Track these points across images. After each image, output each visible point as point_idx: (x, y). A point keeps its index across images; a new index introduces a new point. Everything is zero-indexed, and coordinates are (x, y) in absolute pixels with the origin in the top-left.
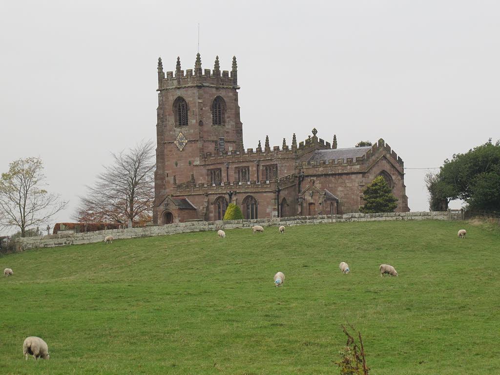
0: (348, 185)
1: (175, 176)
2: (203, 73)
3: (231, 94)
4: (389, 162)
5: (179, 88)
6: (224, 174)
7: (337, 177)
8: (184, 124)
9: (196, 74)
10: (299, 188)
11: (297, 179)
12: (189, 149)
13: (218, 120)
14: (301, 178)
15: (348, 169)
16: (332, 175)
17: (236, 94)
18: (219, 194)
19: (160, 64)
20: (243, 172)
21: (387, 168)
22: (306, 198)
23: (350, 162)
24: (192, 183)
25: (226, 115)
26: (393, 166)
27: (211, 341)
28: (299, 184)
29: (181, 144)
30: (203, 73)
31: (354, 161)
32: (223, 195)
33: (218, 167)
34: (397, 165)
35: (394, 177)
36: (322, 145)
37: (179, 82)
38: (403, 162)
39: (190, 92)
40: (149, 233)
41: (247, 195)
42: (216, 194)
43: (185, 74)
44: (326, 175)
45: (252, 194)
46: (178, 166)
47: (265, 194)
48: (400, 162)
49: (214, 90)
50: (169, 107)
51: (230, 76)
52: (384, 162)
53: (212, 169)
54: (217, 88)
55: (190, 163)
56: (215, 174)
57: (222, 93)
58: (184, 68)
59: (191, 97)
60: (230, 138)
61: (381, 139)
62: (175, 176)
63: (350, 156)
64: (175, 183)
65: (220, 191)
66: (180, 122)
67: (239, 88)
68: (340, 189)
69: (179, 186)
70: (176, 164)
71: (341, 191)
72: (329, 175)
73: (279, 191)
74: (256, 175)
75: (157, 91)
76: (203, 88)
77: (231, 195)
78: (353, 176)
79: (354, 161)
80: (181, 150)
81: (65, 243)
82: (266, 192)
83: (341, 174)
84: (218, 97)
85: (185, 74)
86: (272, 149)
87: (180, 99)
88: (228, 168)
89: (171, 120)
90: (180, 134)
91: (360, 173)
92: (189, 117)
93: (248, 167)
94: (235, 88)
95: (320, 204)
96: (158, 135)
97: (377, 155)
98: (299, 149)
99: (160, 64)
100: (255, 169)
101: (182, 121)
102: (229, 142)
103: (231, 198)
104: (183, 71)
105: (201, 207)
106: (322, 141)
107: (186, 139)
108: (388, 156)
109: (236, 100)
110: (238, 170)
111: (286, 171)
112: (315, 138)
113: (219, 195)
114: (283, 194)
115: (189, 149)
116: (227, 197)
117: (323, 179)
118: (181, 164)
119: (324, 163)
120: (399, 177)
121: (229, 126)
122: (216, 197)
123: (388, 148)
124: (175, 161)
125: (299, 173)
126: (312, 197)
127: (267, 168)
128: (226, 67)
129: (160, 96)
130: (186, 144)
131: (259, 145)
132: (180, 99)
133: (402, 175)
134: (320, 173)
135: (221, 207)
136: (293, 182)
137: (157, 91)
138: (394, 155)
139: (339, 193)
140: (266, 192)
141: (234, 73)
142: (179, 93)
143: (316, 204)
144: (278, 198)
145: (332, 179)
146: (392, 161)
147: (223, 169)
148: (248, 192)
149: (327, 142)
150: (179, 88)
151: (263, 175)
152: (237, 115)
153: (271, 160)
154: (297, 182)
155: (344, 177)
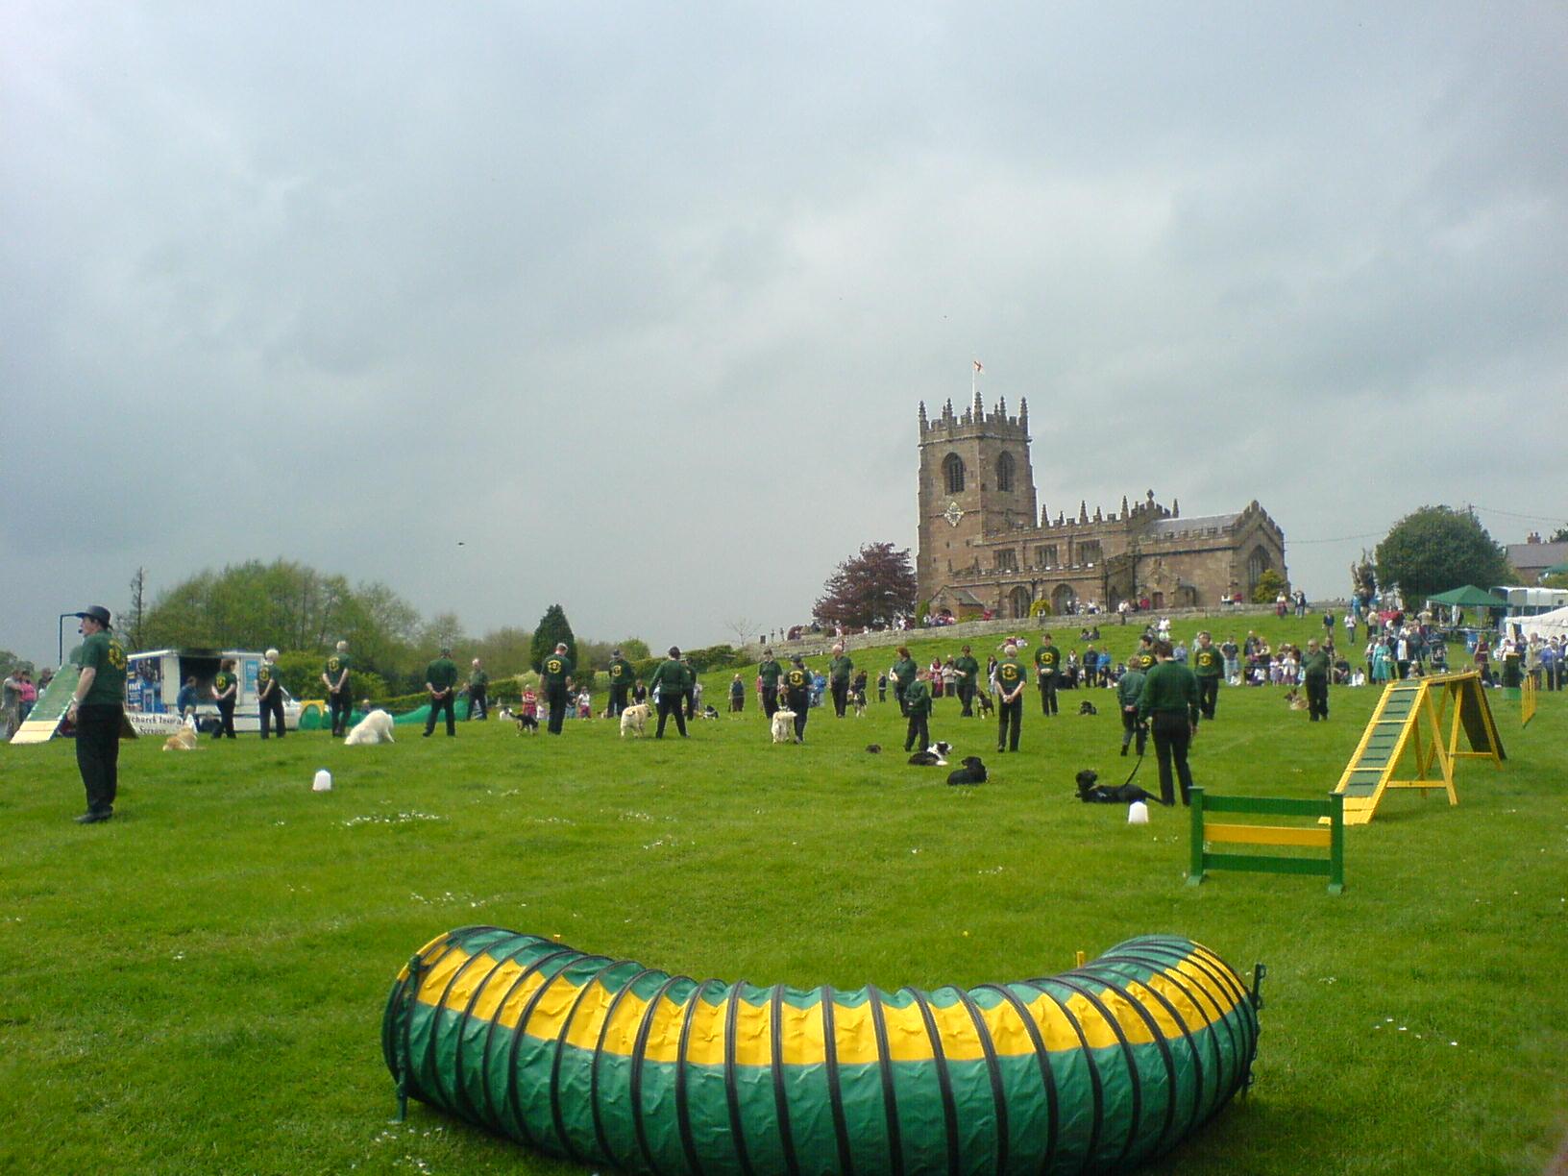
0: (1210, 566)
1: (949, 561)
2: (985, 420)
3: (1020, 449)
4: (1265, 533)
5: (950, 441)
6: (1019, 557)
7: (1193, 555)
8: (957, 491)
9: (1020, 423)
10: (1134, 572)
11: (1131, 559)
12: (966, 523)
13: (1004, 486)
14: (1139, 558)
15: (1212, 543)
16: (1187, 553)
17: (1027, 449)
18: (1018, 583)
19: (922, 409)
20: (1048, 553)
21: (1264, 542)
22: (1148, 585)
23: (1213, 532)
24: (973, 570)
25: (1015, 477)
26: (1271, 539)
27: (699, 880)
28: (1134, 567)
29: (954, 517)
30: (985, 420)
31: (1220, 531)
32: (1023, 585)
33: (1010, 546)
34: (1275, 538)
35: (1272, 555)
36: (1160, 513)
37: (950, 433)
38: (1283, 535)
39: (967, 444)
40: (933, 636)
41: (1059, 583)
42: (1012, 583)
43: (959, 422)
44: (1175, 553)
45: (1066, 583)
46: (951, 547)
47: (1086, 582)
48: (1279, 533)
49: (999, 442)
50: (936, 466)
51: (1018, 423)
52: (1260, 533)
53: (1002, 550)
54: (1003, 440)
55: (968, 543)
56: (1005, 557)
57: (1009, 447)
58: (958, 412)
59: (970, 453)
60: (1021, 508)
61: (1255, 501)
62: (949, 561)
63: (1211, 525)
64: (950, 570)
65: (1018, 579)
66: (952, 488)
67: (1030, 441)
68: (1198, 572)
69: (958, 573)
70: (948, 545)
71: (1198, 575)
72: (1180, 553)
73: (1107, 577)
74: (1067, 557)
75: (919, 446)
76: (955, 442)
77: (1034, 584)
78: (1219, 554)
79: (1220, 531)
80: (955, 525)
81: (814, 651)
82: (1087, 579)
83: (1199, 552)
84: (1005, 453)
85: (959, 422)
86: (1105, 518)
87: (952, 456)
88: (1024, 548)
89: (940, 485)
90: (953, 507)
91: (1229, 549)
92: (965, 480)
93: (1055, 546)
94: (1025, 441)
95: (1172, 593)
96: (921, 506)
97: (1251, 523)
98: (1132, 518)
99: (922, 409)
100: (1065, 547)
101: (955, 485)
102: (1018, 514)
103: (1034, 588)
104: (956, 418)
105: (990, 602)
106: (1159, 507)
107: (962, 510)
108: (1264, 524)
109: (1027, 456)
110: (1040, 551)
111: (1114, 548)
112: (1151, 503)
113: (1015, 586)
114: (1112, 581)
115: (966, 523)
116: (1029, 587)
117: (1169, 559)
118: (955, 545)
119: (1172, 536)
120: (1278, 555)
121: (1019, 489)
122: (1011, 588)
123: (1263, 514)
124: (945, 541)
125: (1133, 552)
126: (1158, 584)
127: (1083, 547)
128: (1013, 412)
129: (923, 452)
130: (962, 517)
131: (1123, 510)
132: (952, 456)
133: (1282, 551)
134: (1164, 551)
135: (1020, 601)
136: (1125, 564)
137: (919, 446)
138: (1271, 523)
139: (1198, 578)
140: (1087, 579)
141: (1024, 419)
142: (950, 448)
143: (1165, 594)
144: (1105, 587)
145: (1186, 559)
146: (1269, 531)
147: (1018, 548)
148: (1060, 580)
149: (1166, 510)
150: (950, 441)
151: (1077, 554)
152: (1029, 476)
153: (1089, 534)
154: (1130, 564)
155: (1204, 554)
